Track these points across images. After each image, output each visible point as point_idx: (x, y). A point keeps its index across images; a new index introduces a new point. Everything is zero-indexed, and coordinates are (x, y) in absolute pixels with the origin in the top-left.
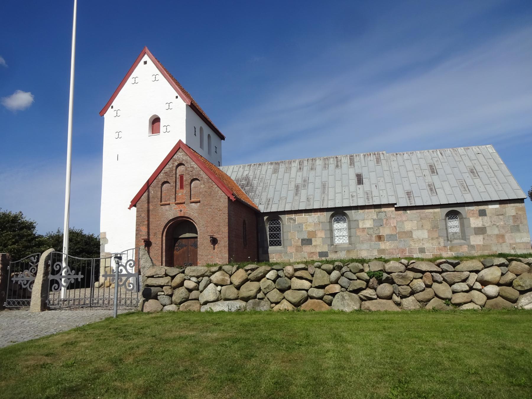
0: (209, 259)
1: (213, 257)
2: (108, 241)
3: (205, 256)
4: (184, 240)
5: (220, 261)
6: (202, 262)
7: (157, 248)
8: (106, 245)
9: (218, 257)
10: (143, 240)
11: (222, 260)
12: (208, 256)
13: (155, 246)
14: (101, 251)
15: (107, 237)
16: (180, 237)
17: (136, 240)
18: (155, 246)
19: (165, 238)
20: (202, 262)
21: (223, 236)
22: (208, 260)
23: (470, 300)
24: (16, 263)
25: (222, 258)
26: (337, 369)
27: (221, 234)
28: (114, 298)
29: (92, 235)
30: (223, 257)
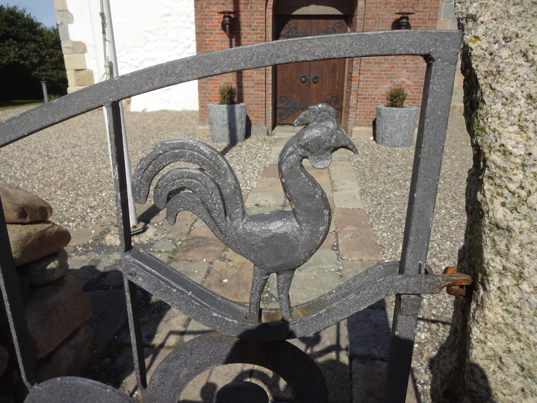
0: (384, 71)
1: (393, 67)
2: (72, 17)
3: (375, 64)
4: (300, 21)
5: (409, 78)
6: (367, 78)
7: (255, 37)
8: (70, 26)
9: (407, 68)
10: (223, 15)
11: (416, 75)
12: (382, 63)
13: (249, 34)
14: (61, 39)
15: (70, 8)
16: (295, 13)
17: (196, 15)
18: (249, 34)
19: (271, 14)
20: (367, 78)
21: (425, 15)
22: (381, 75)
23: (78, 72)
24: (135, 201)
25: (415, 71)
26: (41, 168)
27: (421, 12)
28: (281, 309)
29: (15, 7)
30: (418, 68)
